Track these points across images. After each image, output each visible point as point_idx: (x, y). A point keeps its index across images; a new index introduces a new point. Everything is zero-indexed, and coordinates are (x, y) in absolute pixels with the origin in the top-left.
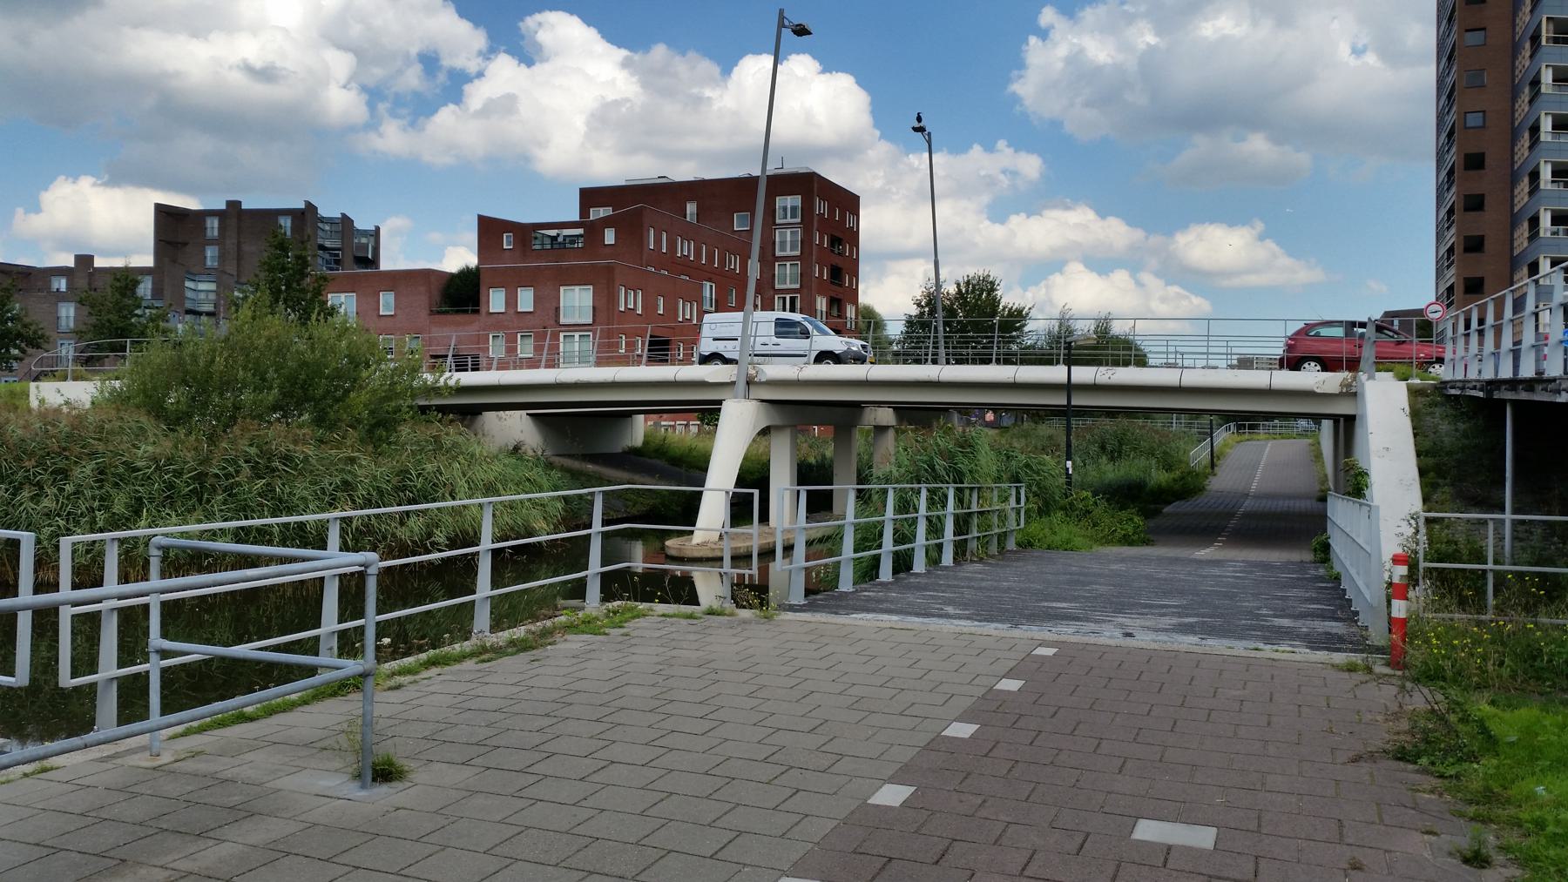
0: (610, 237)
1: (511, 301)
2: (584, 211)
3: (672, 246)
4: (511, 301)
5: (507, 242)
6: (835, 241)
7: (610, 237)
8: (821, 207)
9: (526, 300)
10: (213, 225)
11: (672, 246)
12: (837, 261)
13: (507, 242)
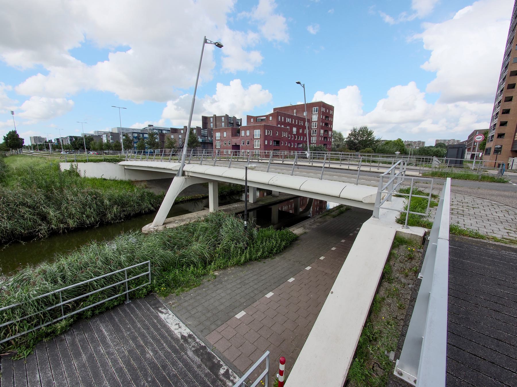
0: (271, 118)
1: (245, 134)
3: (285, 120)
4: (245, 134)
7: (271, 118)
8: (323, 109)
10: (212, 119)
11: (285, 120)
12: (327, 122)
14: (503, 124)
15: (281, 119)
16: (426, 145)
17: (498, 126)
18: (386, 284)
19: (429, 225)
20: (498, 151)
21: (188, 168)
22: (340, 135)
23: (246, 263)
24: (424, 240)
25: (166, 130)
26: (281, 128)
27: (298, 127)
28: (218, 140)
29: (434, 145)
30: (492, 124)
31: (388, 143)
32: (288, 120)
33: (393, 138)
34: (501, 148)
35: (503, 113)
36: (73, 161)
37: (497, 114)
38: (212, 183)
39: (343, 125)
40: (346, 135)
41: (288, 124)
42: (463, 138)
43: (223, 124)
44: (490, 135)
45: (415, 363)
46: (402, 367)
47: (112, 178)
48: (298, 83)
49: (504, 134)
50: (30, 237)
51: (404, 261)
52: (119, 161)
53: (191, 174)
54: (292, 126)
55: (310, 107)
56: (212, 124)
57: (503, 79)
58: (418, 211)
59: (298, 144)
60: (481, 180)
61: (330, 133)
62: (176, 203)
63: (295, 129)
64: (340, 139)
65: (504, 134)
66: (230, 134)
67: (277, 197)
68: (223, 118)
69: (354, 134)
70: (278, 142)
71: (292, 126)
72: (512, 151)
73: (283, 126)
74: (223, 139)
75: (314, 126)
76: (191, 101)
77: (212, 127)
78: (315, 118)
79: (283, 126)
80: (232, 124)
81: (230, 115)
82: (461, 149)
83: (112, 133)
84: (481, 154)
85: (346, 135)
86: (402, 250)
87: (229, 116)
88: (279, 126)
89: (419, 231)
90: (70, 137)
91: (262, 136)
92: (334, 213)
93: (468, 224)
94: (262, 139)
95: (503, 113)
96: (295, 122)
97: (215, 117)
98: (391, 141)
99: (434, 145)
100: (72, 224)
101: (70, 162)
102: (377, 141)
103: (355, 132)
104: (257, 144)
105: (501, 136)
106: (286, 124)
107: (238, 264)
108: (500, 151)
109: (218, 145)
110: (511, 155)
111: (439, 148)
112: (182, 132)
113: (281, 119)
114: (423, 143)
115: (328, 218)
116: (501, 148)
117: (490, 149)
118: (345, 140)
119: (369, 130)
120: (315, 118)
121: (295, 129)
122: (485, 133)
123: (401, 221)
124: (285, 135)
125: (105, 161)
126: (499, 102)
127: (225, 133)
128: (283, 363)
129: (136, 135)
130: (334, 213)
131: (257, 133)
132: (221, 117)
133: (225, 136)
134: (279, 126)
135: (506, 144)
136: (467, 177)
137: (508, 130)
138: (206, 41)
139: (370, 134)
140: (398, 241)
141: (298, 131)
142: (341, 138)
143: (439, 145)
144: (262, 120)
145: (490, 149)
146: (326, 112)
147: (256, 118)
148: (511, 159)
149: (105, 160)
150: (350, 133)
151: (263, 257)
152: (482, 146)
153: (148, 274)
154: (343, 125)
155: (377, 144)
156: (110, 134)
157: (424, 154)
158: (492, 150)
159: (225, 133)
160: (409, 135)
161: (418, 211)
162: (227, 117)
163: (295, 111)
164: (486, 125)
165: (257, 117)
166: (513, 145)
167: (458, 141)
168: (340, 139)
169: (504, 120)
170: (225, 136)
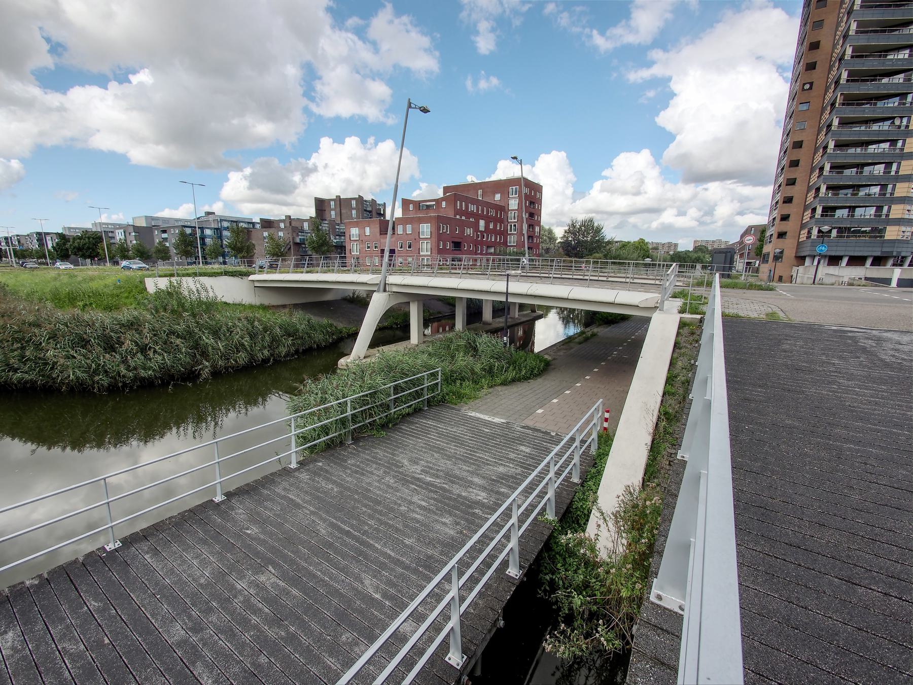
0: (444, 204)
1: (405, 230)
2: (445, 193)
3: (467, 207)
4: (405, 230)
5: (411, 207)
6: (532, 203)
7: (444, 204)
9: (409, 228)
10: (332, 203)
11: (467, 207)
12: (533, 211)
13: (411, 207)
14: (785, 218)
15: (461, 205)
16: (680, 249)
17: (777, 221)
18: (677, 350)
19: (704, 314)
20: (778, 257)
21: (392, 279)
22: (550, 232)
23: (514, 381)
24: (701, 321)
25: (228, 221)
26: (460, 220)
27: (488, 219)
28: (355, 241)
29: (691, 249)
30: (771, 218)
31: (624, 245)
32: (472, 208)
33: (633, 238)
34: (782, 252)
35: (784, 202)
36: (172, 275)
37: (777, 203)
38: (416, 303)
39: (557, 214)
40: (559, 233)
41: (472, 214)
42: (733, 239)
43: (354, 212)
44: (768, 234)
45: (681, 582)
46: (661, 589)
47: (237, 301)
48: (515, 158)
49: (785, 233)
50: (191, 376)
51: (689, 337)
52: (247, 274)
53: (395, 289)
54: (477, 217)
55: (502, 186)
56: (333, 213)
57: (784, 152)
58: (694, 306)
59: (488, 247)
60: (748, 289)
61: (537, 229)
62: (380, 329)
63: (482, 223)
64: (550, 239)
65: (785, 233)
66: (378, 230)
67: (490, 324)
68: (354, 203)
69: (573, 230)
70: (457, 245)
71: (477, 217)
72: (796, 257)
73: (463, 218)
74: (364, 238)
75: (512, 218)
76: (393, 187)
77: (333, 216)
78: (513, 204)
79: (463, 218)
80: (370, 212)
81: (368, 197)
82: (729, 255)
83: (137, 229)
84: (758, 262)
85: (559, 233)
86: (686, 330)
87: (365, 198)
88: (458, 217)
89: (699, 317)
90: (39, 234)
91: (433, 235)
92: (577, 340)
93: (731, 311)
94: (435, 239)
95: (784, 202)
96: (483, 211)
97: (339, 200)
98: (629, 242)
99: (691, 249)
100: (242, 358)
101: (165, 276)
102: (609, 242)
103: (574, 227)
104: (426, 249)
105: (781, 235)
106: (469, 214)
107: (504, 383)
108: (781, 257)
109: (354, 250)
110: (795, 262)
111: (700, 254)
112: (282, 225)
113: (461, 205)
114: (676, 245)
115: (572, 345)
116: (782, 252)
117: (768, 254)
118: (559, 240)
119: (596, 225)
120: (513, 204)
121: (482, 223)
122: (761, 231)
123: (680, 312)
124: (469, 231)
125: (226, 275)
126: (780, 186)
127: (367, 230)
128: (608, 412)
129: (188, 231)
130: (577, 340)
131: (426, 229)
132: (349, 200)
133: (368, 233)
134: (458, 217)
135: (788, 246)
136: (734, 286)
137: (790, 227)
138: (410, 106)
139: (598, 230)
140: (682, 325)
141: (487, 226)
142: (552, 238)
143: (700, 249)
144: (428, 207)
145: (768, 254)
146: (531, 194)
147: (418, 205)
148: (795, 269)
149: (226, 273)
150: (567, 228)
151: (526, 378)
152: (759, 252)
153: (437, 384)
154: (557, 214)
155: (608, 247)
156: (131, 229)
157: (684, 260)
158: (771, 256)
159: (367, 230)
160: (649, 230)
161: (694, 306)
162: (360, 200)
163: (480, 192)
164: (762, 219)
165: (420, 202)
166: (797, 249)
167: (726, 242)
168: (550, 239)
169: (785, 212)
170: (368, 233)
